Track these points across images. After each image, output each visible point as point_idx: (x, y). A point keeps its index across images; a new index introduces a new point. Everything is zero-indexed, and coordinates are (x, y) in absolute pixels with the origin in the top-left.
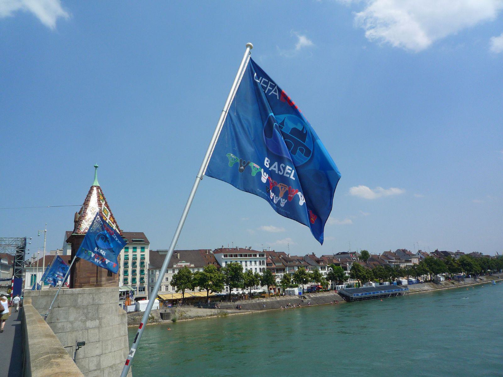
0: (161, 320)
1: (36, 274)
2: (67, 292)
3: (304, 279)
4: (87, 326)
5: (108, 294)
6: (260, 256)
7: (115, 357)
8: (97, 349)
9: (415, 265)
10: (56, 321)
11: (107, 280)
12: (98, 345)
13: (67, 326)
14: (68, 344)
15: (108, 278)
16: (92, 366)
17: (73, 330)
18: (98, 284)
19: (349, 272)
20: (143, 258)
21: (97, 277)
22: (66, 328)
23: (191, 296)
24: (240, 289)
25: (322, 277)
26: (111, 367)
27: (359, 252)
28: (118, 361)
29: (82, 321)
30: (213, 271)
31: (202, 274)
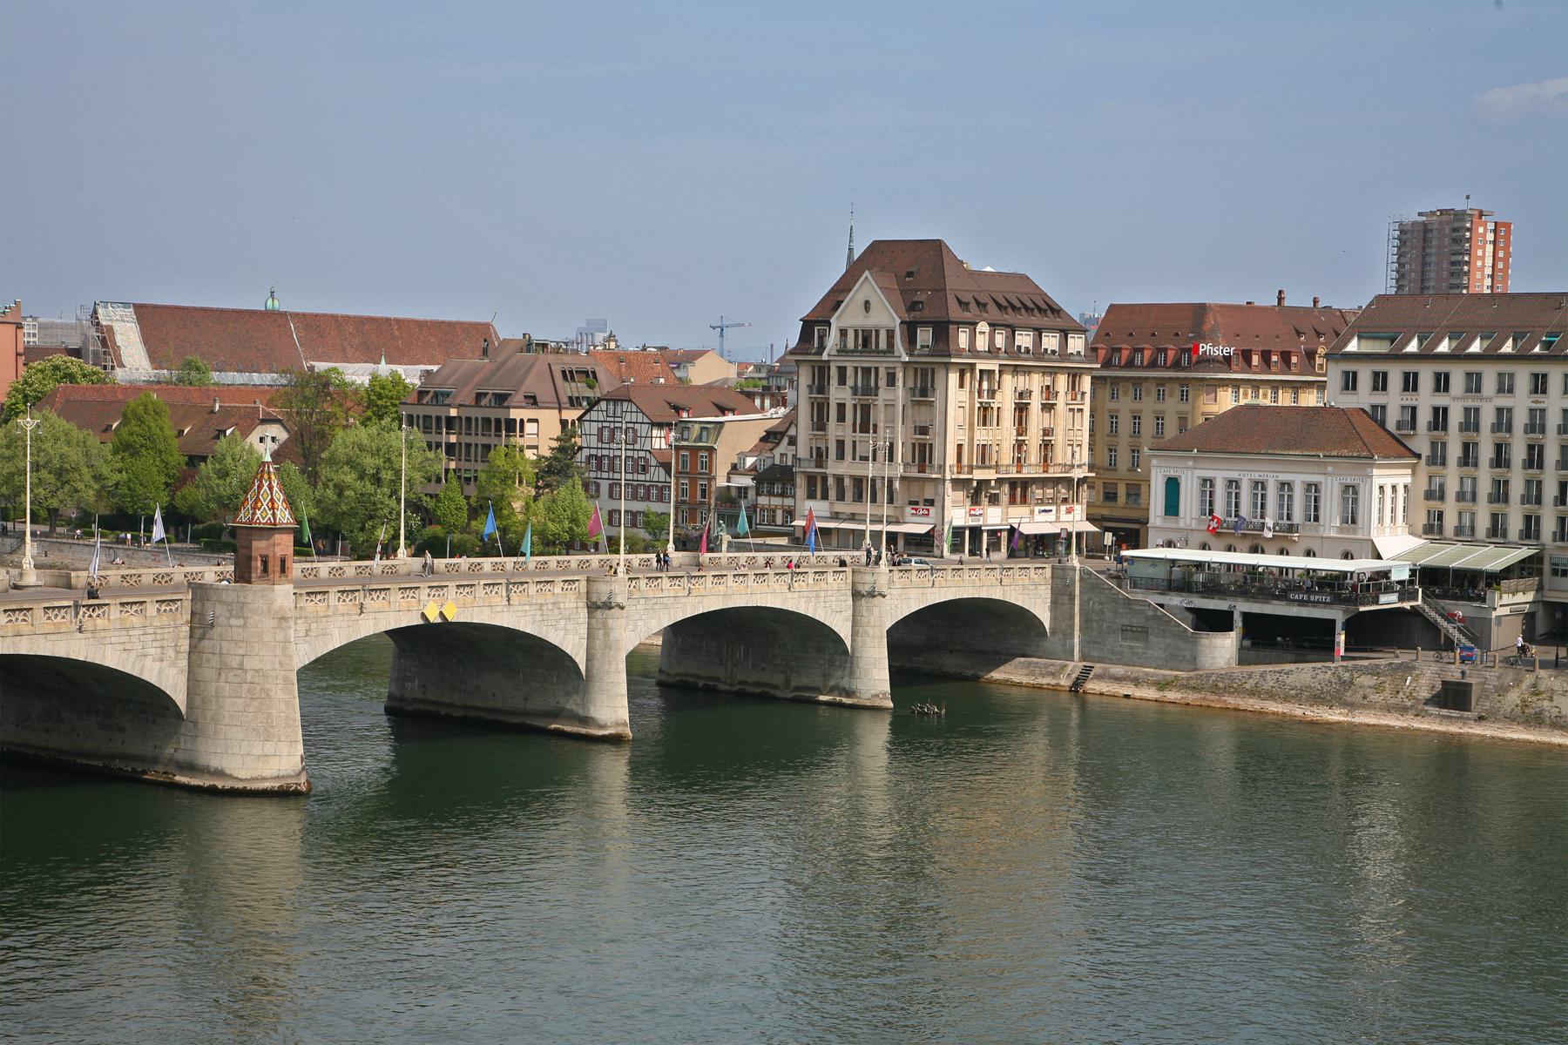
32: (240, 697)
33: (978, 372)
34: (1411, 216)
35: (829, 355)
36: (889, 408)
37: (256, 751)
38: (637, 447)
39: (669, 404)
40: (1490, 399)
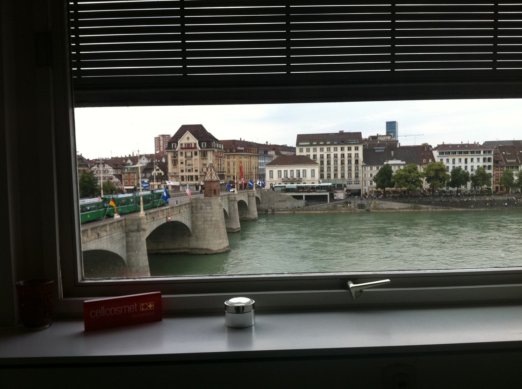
15: (144, 206)
18: (211, 196)
20: (357, 155)
26: (216, 221)
32: (212, 228)
33: (215, 152)
34: (157, 136)
35: (178, 149)
36: (196, 161)
37: (218, 242)
38: (109, 174)
39: (114, 164)
40: (332, 152)
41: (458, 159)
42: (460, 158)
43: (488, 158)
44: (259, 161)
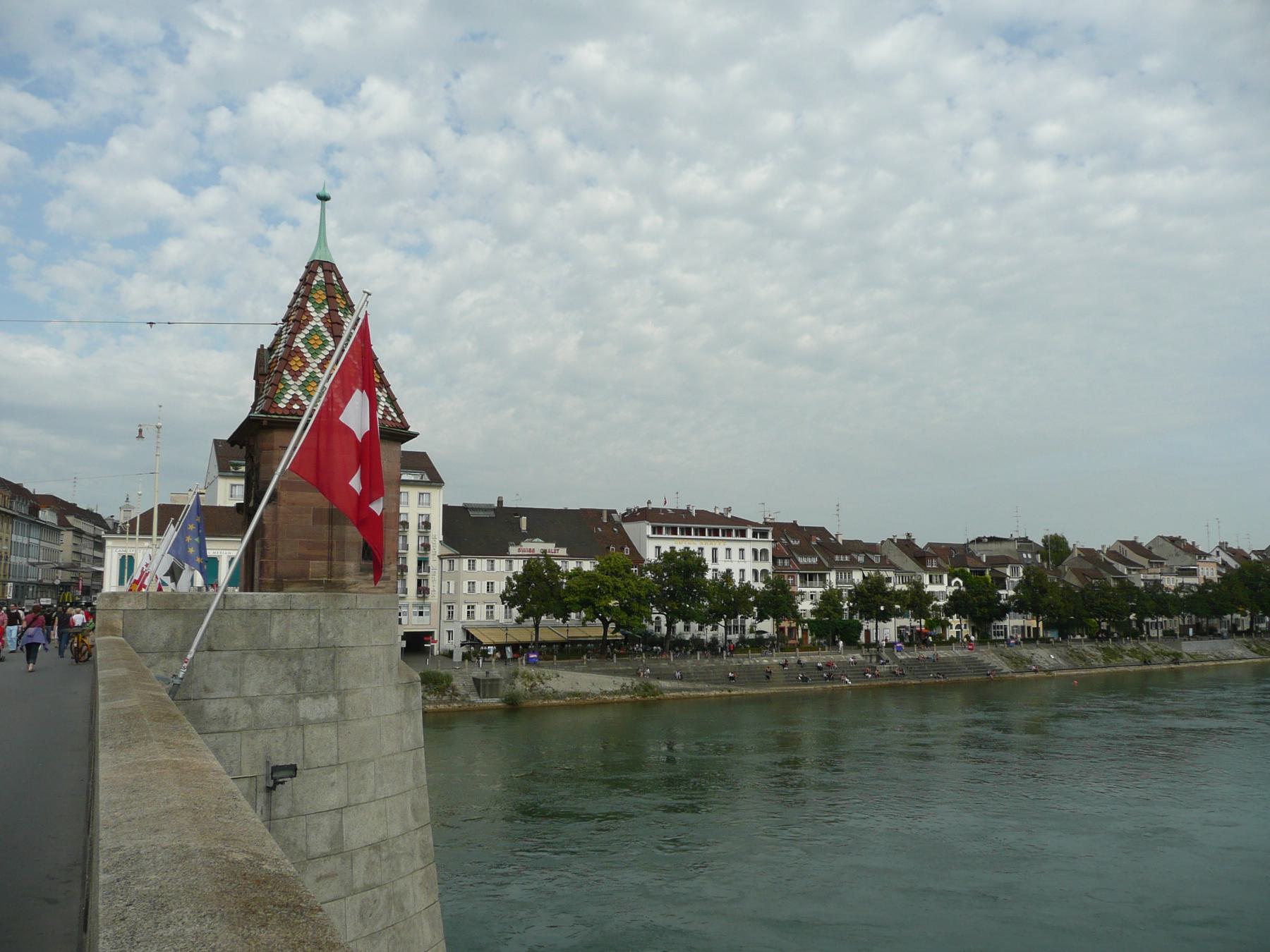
0: (474, 698)
1: (134, 554)
2: (237, 603)
3: (882, 608)
4: (301, 715)
5: (365, 616)
6: (754, 535)
7: (386, 816)
8: (334, 787)
9: (1208, 583)
10: (203, 695)
11: (361, 570)
12: (334, 776)
13: (237, 713)
14: (241, 770)
15: (363, 563)
16: (318, 844)
17: (257, 726)
19: (1012, 593)
21: (330, 559)
22: (235, 721)
23: (562, 639)
24: (694, 626)
25: (934, 602)
26: (376, 847)
27: (1038, 540)
28: (396, 830)
29: (284, 699)
30: (623, 572)
31: (588, 576)
41: (725, 550)
42: (743, 548)
43: (761, 550)
44: (14, 538)
